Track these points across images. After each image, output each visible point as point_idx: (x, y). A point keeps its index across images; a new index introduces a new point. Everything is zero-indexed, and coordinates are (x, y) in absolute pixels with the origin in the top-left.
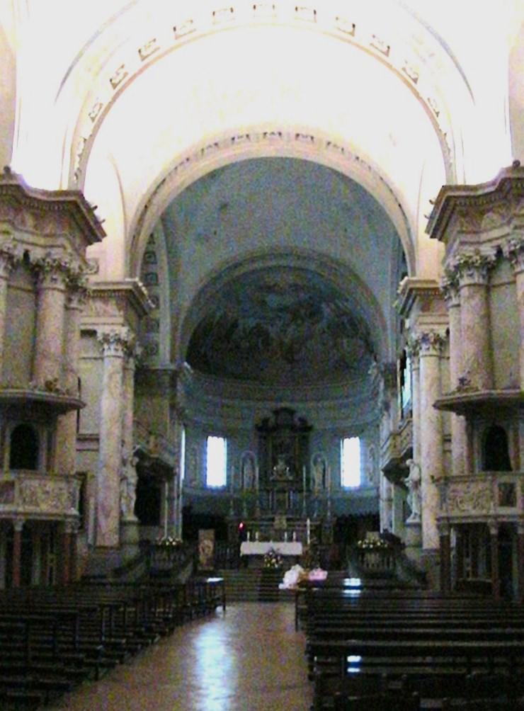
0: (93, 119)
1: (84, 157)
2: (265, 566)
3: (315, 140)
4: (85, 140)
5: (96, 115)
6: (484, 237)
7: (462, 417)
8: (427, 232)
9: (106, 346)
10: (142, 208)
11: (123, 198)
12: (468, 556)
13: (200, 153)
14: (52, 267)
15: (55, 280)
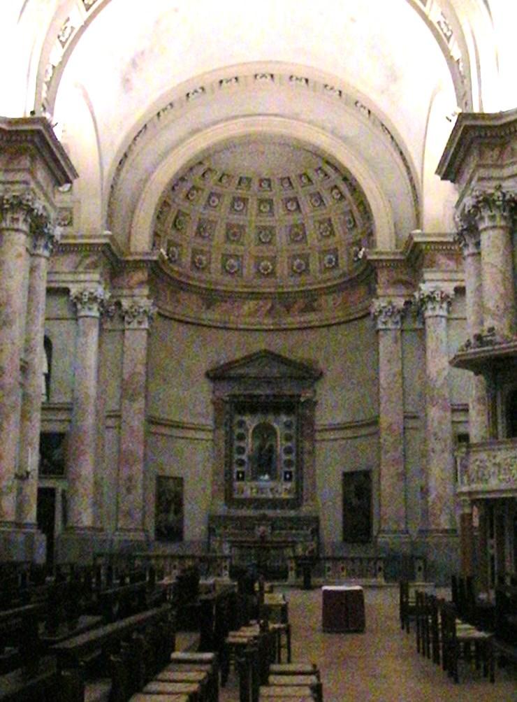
0: (63, 44)
1: (52, 85)
2: (80, 659)
3: (309, 81)
4: (54, 67)
5: (67, 39)
6: (506, 172)
7: (482, 378)
8: (438, 172)
9: (79, 306)
10: (122, 155)
11: (97, 136)
12: (492, 536)
13: (185, 98)
14: (11, 204)
15: (17, 220)
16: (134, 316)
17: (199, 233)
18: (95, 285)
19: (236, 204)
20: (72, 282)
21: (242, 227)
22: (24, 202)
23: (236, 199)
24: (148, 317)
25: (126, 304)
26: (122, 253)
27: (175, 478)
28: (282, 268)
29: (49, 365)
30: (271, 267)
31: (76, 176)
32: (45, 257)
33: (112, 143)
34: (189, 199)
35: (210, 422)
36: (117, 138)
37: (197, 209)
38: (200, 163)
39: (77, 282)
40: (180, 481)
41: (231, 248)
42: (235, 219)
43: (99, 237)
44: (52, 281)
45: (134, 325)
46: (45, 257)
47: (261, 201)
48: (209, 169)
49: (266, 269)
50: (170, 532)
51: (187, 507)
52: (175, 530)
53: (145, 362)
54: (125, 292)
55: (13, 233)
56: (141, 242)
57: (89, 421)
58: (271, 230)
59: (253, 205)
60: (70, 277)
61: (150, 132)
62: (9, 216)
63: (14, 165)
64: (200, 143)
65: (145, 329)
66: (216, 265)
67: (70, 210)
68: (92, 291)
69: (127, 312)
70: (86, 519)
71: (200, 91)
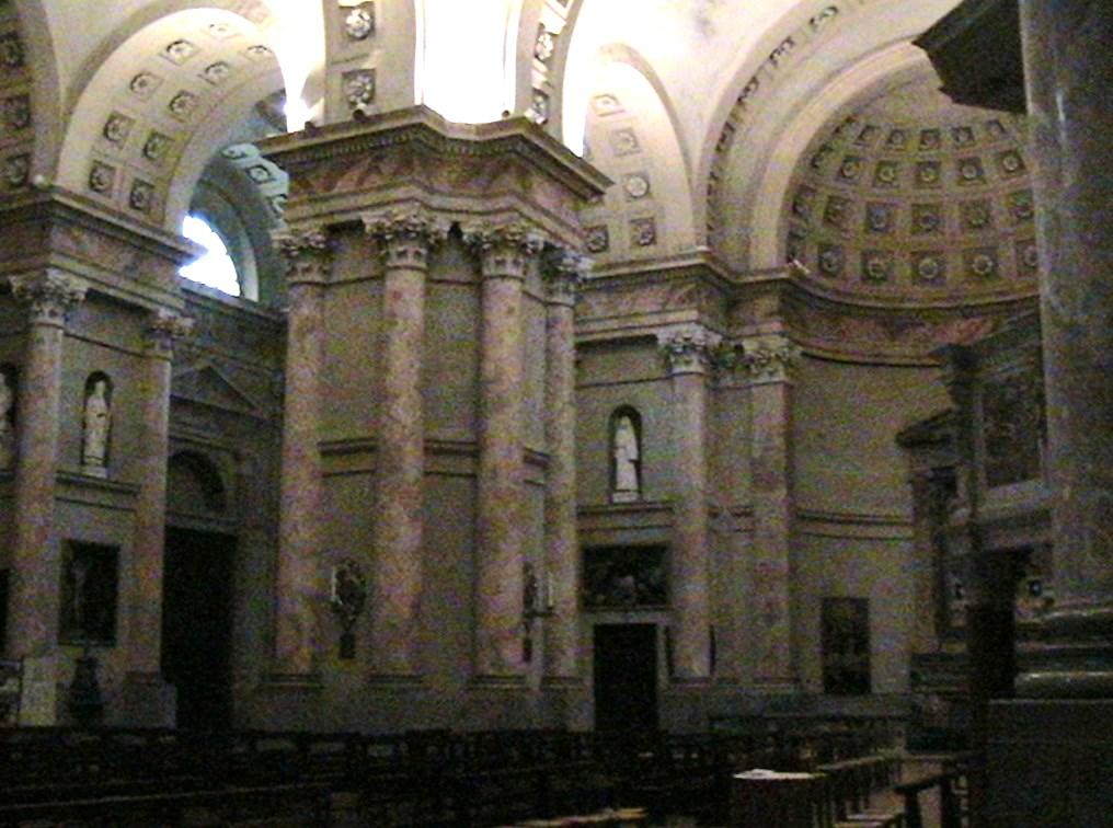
16: (763, 365)
17: (870, 227)
18: (693, 327)
19: (923, 174)
20: (659, 325)
21: (917, 207)
22: (509, 237)
23: (922, 166)
24: (783, 363)
25: (749, 347)
26: (737, 274)
27: (853, 601)
28: (955, 266)
29: (639, 447)
30: (990, 264)
31: (608, 182)
32: (567, 305)
33: (700, 116)
34: (844, 176)
35: (904, 510)
36: (705, 111)
37: (861, 192)
38: (849, 120)
39: (666, 324)
40: (861, 605)
41: (926, 240)
42: (925, 195)
43: (689, 256)
44: (583, 334)
45: (764, 378)
46: (567, 305)
47: (962, 163)
48: (869, 128)
49: (983, 266)
50: (851, 680)
51: (877, 642)
52: (857, 677)
53: (88, 430)
54: (747, 330)
55: (498, 281)
56: (766, 253)
57: (696, 524)
58: (983, 204)
59: (949, 172)
60: (655, 320)
61: (764, 87)
62: (492, 259)
63: (495, 188)
64: (841, 93)
65: (779, 383)
66: (903, 270)
67: (651, 221)
68: (687, 336)
69: (752, 360)
70: (698, 667)
71: (831, 13)
